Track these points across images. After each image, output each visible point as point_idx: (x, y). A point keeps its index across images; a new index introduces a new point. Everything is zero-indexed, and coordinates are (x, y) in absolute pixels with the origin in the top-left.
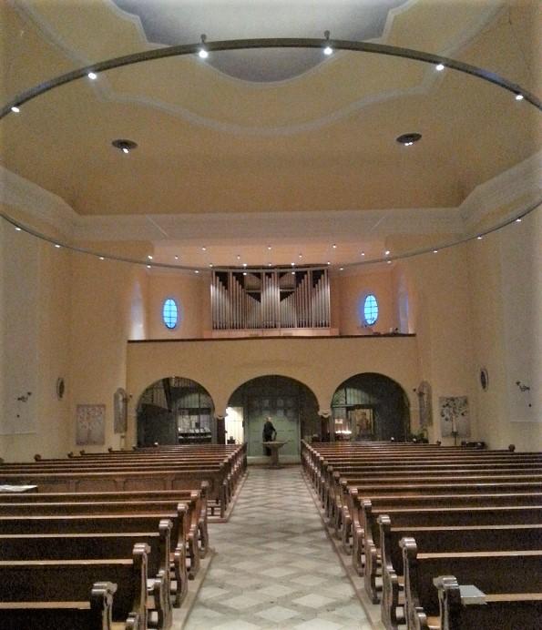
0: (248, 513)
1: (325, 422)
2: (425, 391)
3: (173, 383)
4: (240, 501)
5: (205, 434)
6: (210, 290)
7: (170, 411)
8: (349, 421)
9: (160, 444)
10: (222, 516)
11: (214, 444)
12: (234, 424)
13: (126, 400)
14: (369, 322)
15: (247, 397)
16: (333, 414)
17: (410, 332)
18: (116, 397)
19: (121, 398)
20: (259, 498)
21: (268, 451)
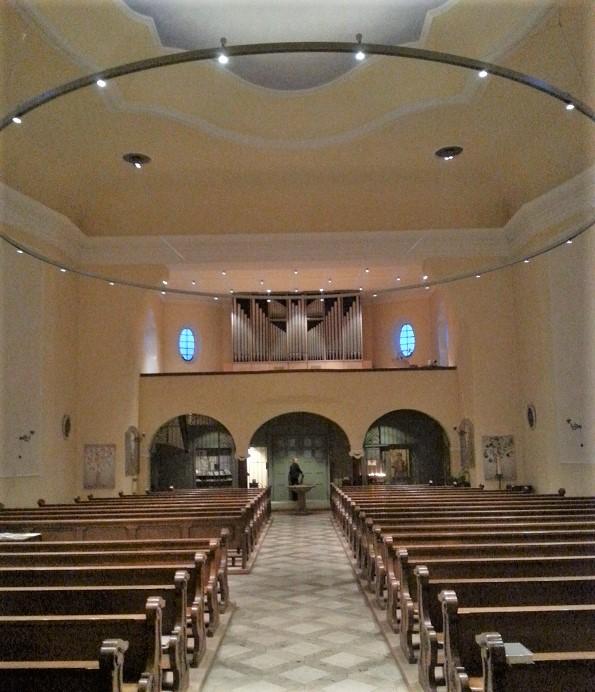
0: (273, 564)
1: (356, 463)
2: (466, 430)
3: (190, 421)
4: (263, 550)
5: (226, 477)
6: (230, 319)
7: (187, 452)
8: (383, 462)
9: (175, 487)
10: (243, 566)
11: (235, 488)
12: (257, 465)
13: (138, 440)
14: (405, 354)
15: (271, 437)
16: (366, 455)
17: (450, 365)
18: (127, 436)
19: (133, 437)
20: (285, 547)
21: (294, 496)
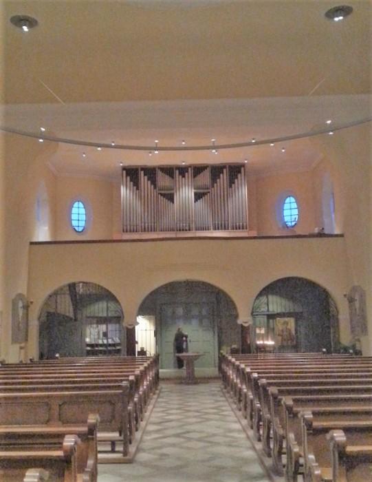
0: (160, 448)
1: (244, 331)
2: (357, 297)
3: (81, 290)
4: (151, 428)
5: (114, 345)
6: (120, 190)
7: (76, 320)
8: (270, 331)
9: (61, 356)
10: (125, 453)
11: (124, 355)
12: (145, 333)
13: (26, 307)
14: (289, 224)
15: (157, 305)
16: (254, 324)
17: (337, 232)
18: (14, 303)
19: (21, 304)
20: (173, 424)
21: (180, 363)
